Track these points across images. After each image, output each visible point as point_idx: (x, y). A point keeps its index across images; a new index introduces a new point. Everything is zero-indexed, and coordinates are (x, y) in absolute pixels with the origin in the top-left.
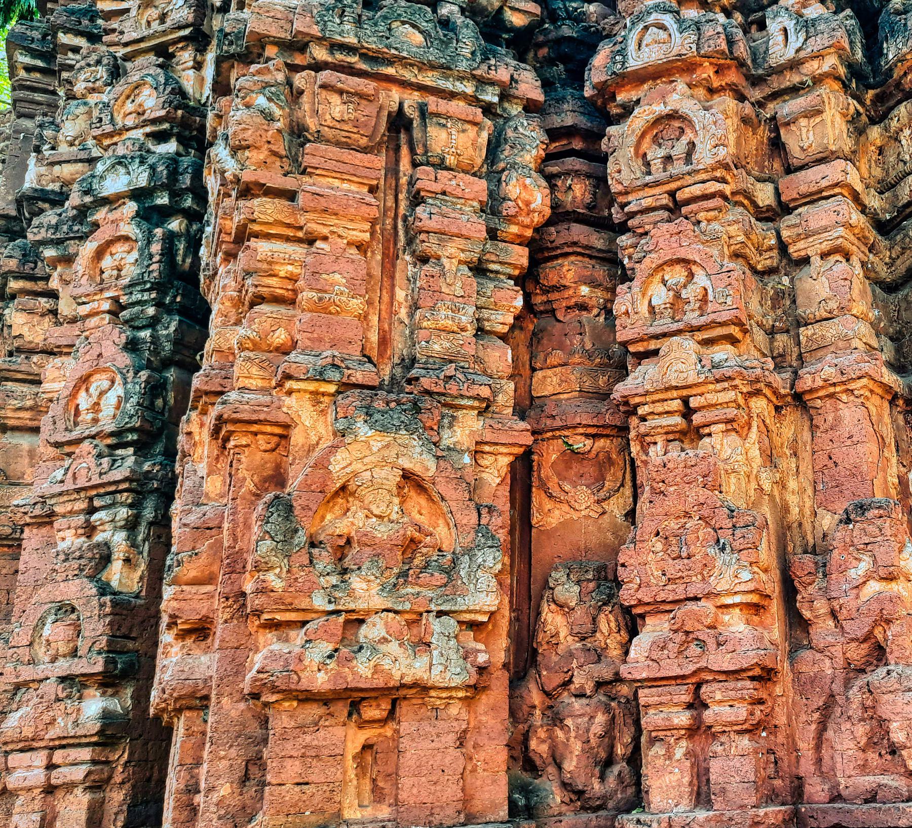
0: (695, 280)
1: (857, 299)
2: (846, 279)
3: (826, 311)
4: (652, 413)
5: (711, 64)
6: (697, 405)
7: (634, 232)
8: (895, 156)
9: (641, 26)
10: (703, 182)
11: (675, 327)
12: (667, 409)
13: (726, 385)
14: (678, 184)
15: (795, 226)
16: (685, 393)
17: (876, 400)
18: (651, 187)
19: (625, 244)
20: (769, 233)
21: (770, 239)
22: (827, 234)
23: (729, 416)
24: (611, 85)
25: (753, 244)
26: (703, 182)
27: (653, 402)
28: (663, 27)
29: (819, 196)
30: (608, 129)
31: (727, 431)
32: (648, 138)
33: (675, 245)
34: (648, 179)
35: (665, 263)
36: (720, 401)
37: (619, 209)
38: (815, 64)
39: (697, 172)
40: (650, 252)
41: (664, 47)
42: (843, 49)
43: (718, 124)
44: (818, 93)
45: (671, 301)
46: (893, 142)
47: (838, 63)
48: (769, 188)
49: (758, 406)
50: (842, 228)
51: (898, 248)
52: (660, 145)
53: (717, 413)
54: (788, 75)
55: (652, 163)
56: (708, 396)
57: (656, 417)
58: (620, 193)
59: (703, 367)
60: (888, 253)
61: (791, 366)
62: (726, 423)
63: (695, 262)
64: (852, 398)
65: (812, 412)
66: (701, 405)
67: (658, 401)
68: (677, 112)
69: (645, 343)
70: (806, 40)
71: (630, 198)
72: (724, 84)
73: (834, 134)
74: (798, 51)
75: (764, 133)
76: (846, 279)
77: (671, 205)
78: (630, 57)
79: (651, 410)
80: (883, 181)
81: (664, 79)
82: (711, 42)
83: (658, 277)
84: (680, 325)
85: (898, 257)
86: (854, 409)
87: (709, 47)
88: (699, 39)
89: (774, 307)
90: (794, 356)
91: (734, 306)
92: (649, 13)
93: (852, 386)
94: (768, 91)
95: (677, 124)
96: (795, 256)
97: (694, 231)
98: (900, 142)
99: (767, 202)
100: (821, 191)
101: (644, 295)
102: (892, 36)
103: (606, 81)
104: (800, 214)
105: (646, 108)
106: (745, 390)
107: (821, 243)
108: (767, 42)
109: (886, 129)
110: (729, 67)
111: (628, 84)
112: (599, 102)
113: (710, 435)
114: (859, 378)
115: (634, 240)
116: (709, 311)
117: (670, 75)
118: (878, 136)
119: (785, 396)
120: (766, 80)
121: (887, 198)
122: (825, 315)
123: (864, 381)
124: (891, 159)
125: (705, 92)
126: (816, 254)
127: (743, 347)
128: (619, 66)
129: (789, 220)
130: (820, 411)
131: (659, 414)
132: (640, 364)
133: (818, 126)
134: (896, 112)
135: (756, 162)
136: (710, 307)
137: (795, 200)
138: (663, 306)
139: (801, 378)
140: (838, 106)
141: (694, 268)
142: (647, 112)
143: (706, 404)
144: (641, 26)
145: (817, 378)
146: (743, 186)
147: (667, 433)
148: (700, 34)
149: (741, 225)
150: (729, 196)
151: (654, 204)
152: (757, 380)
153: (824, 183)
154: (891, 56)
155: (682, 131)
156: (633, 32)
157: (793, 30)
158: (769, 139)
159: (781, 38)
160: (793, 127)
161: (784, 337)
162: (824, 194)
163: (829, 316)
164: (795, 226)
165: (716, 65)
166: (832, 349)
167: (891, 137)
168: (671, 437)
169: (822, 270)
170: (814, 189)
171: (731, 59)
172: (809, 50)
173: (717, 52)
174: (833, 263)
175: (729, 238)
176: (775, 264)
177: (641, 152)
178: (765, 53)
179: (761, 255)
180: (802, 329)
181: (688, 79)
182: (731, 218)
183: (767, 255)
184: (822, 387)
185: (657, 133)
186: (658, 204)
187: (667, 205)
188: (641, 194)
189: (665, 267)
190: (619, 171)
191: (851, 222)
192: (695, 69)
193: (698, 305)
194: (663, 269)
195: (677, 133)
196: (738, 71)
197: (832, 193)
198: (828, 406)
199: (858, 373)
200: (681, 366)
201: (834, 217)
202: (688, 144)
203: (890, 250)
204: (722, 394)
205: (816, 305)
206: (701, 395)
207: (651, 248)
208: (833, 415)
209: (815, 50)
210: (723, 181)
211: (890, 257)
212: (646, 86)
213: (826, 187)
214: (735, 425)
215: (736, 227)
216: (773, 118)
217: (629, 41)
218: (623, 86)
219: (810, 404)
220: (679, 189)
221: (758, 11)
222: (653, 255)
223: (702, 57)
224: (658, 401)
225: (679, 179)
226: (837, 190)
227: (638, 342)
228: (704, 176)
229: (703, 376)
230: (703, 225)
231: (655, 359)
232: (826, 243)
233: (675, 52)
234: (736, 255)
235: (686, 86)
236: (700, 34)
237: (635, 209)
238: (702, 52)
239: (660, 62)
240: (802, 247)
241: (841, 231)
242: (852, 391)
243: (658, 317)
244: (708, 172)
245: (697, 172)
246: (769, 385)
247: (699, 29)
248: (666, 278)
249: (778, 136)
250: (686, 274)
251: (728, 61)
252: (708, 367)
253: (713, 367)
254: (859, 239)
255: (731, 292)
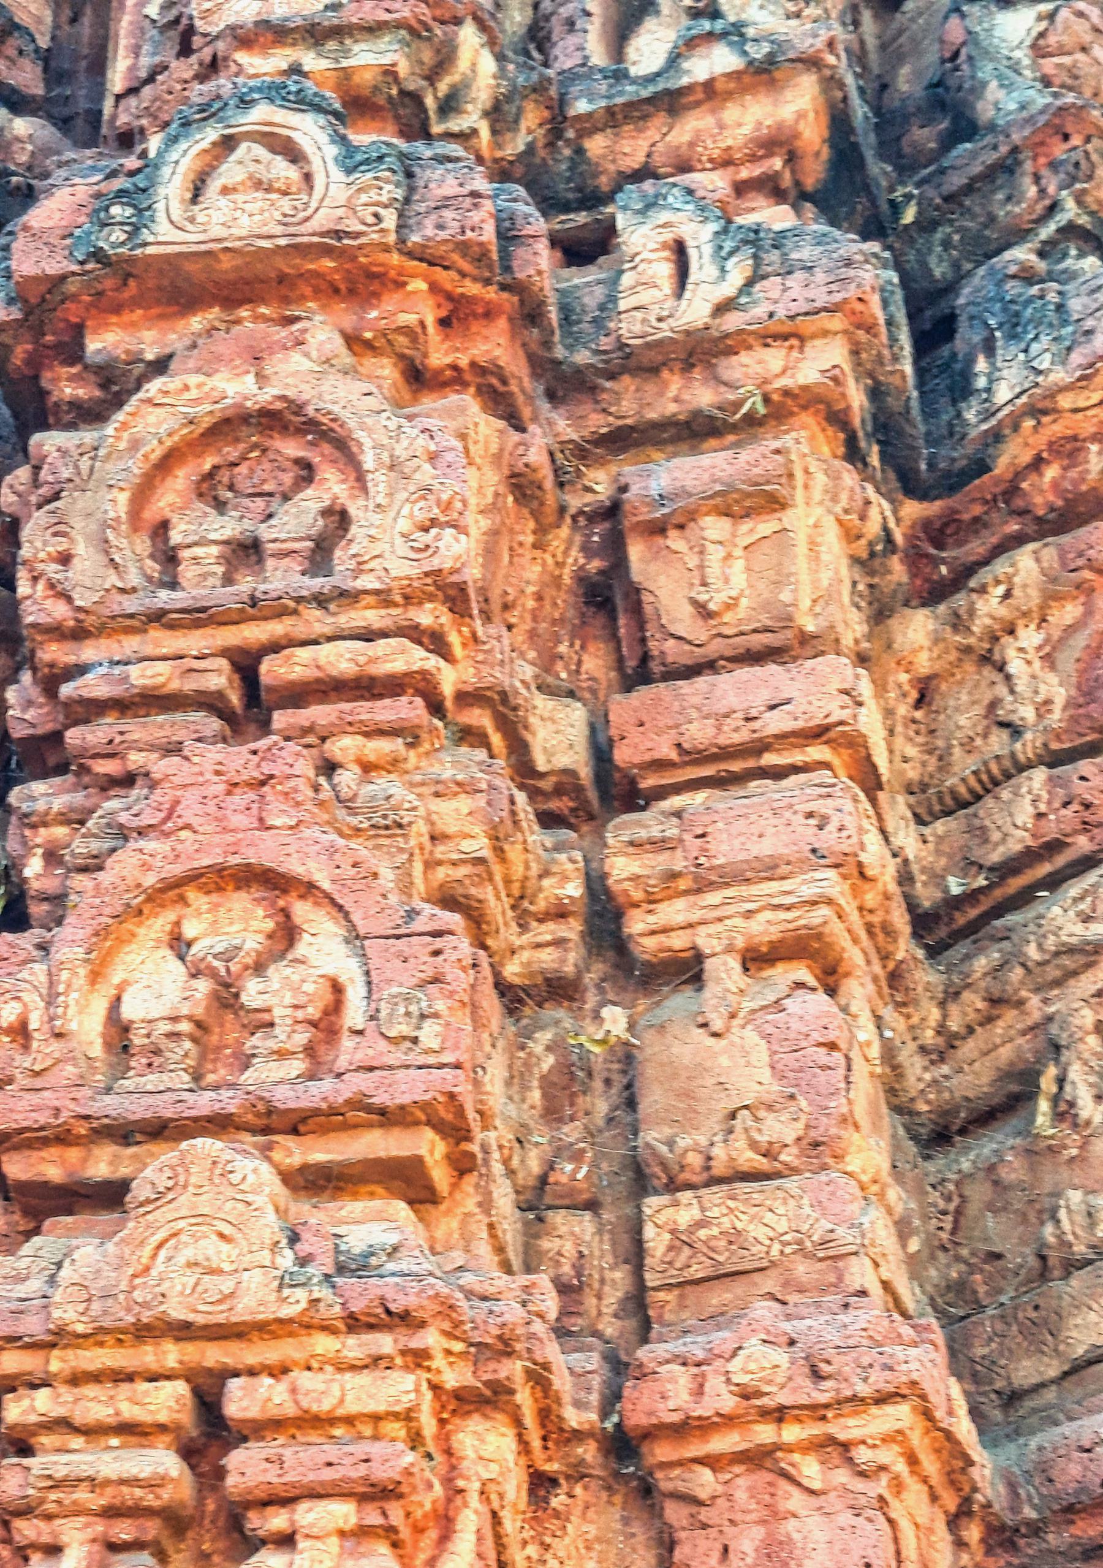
0: (301, 949)
1: (863, 1120)
2: (832, 1046)
3: (753, 1145)
4: (64, 1425)
5: (434, 288)
6: (254, 1413)
7: (84, 770)
8: (979, 710)
9: (211, 134)
10: (368, 636)
11: (204, 1103)
12: (129, 1412)
13: (385, 1343)
14: (276, 629)
15: (660, 845)
16: (214, 1355)
17: (916, 1493)
18: (172, 626)
19: (41, 806)
20: (563, 857)
21: (565, 878)
22: (774, 886)
23: (382, 1473)
24: (74, 298)
25: (508, 881)
26: (368, 636)
27: (76, 1379)
28: (292, 153)
29: (751, 763)
30: (36, 438)
31: (362, 1532)
32: (182, 478)
33: (239, 820)
34: (164, 598)
35: (193, 878)
36: (352, 1407)
37: (35, 693)
38: (774, 359)
39: (348, 597)
40: (141, 832)
41: (285, 204)
42: (870, 328)
43: (441, 463)
44: (777, 444)
45: (199, 1012)
46: (970, 667)
47: (847, 367)
48: (576, 715)
49: (488, 1451)
50: (831, 874)
51: (974, 1001)
52: (220, 506)
53: (332, 1452)
54: (675, 383)
55: (185, 554)
56: (305, 1380)
57: (77, 1442)
58: (56, 632)
59: (303, 1261)
60: (935, 1014)
61: (597, 1334)
62: (363, 1499)
63: (308, 889)
64: (842, 1476)
65: (675, 1513)
66: (274, 1412)
67: (96, 1377)
68: (298, 408)
69: (73, 1154)
70: (750, 283)
71: (88, 652)
72: (464, 362)
73: (815, 586)
74: (723, 308)
75: (566, 553)
76: (832, 1046)
77: (235, 699)
78: (161, 216)
79: (59, 1412)
80: (924, 787)
81: (263, 310)
82: (448, 214)
83: (159, 924)
84: (229, 1102)
85: (971, 1030)
86: (846, 1518)
87: (441, 227)
88: (407, 201)
89: (552, 1114)
90: (613, 1297)
91: (448, 1058)
92: (245, 103)
93: (847, 1428)
94: (598, 423)
95: (291, 448)
96: (647, 947)
97: (316, 788)
98: (1001, 667)
99: (564, 760)
100: (760, 747)
101: (96, 976)
102: (1013, 336)
103: (63, 278)
104: (678, 814)
105: (193, 380)
106: (451, 1379)
107: (749, 914)
108: (615, 281)
109: (958, 623)
110: (489, 314)
111: (135, 303)
112: (20, 354)
113: (286, 1541)
114: (882, 1399)
115: (78, 798)
116: (342, 1063)
117: (286, 301)
118: (926, 643)
119: (578, 1435)
120: (593, 390)
121: (940, 839)
122: (749, 1159)
123: (901, 1415)
124: (963, 721)
125: (397, 375)
126: (729, 949)
127: (447, 1226)
128: (118, 235)
129: (639, 824)
130: (704, 1514)
131: (93, 1432)
132: (36, 1231)
133: (765, 546)
134: (1000, 567)
135: (532, 634)
136: (348, 1052)
137: (660, 765)
138: (165, 1027)
139: (643, 1374)
140: (835, 499)
141: (302, 910)
142: (194, 394)
143: (290, 1410)
144: (211, 134)
145: (715, 1383)
146: (500, 676)
147: (111, 1513)
148: (411, 189)
149: (481, 800)
150: (449, 704)
151: (175, 685)
152: (505, 1347)
153: (776, 723)
154: (1003, 394)
155: (306, 472)
156: (183, 145)
157: (708, 250)
158: (581, 578)
159: (664, 270)
160: (675, 541)
161: (584, 1225)
162: (770, 759)
163: (763, 1164)
164: (660, 845)
165: (449, 297)
166: (769, 1283)
167: (967, 650)
168: (124, 1531)
169: (747, 1005)
170: (737, 738)
171: (504, 287)
172: (760, 311)
173: (463, 247)
174: (782, 989)
175: (433, 838)
176: (569, 969)
177: (151, 514)
178: (602, 308)
179: (523, 927)
180: (652, 1203)
181: (349, 321)
182: (447, 774)
183: (547, 931)
184: (728, 1421)
185: (216, 468)
186: (190, 685)
187: (220, 694)
188: (131, 644)
189: (191, 894)
190: (65, 559)
191: (863, 857)
192: (376, 295)
193: (302, 1037)
194: (182, 900)
195: (288, 478)
196: (513, 335)
197: (797, 757)
198: (741, 1495)
199: (879, 1380)
200: (211, 1249)
201: (807, 831)
202: (326, 513)
203: (942, 1004)
204: (363, 1379)
205: (714, 1123)
206: (279, 1371)
207: (147, 820)
208: (759, 1532)
209: (781, 313)
210: (436, 643)
211: (941, 1030)
212: (196, 322)
213: (782, 737)
214: (396, 1514)
215: (464, 803)
216: (612, 511)
217: (166, 171)
218: (117, 309)
219: (665, 1481)
220: (275, 647)
221: (577, 210)
222: (150, 845)
223: (410, 255)
224: (96, 1377)
225: (282, 613)
226: (817, 752)
227: (45, 1142)
228: (371, 617)
229: (301, 1294)
230: (347, 778)
231: (106, 1218)
232: (768, 915)
233: (321, 221)
234: (448, 901)
235: (339, 341)
236: (411, 189)
237: (102, 691)
238: (415, 238)
239: (266, 244)
240: (680, 919)
241: (830, 882)
242: (846, 1446)
243: (138, 1062)
244: (389, 603)
245: (348, 597)
246: (539, 1377)
247: (410, 175)
248: (190, 930)
249: (619, 563)
250: (270, 925)
251: (491, 293)
252: (324, 1264)
253: (341, 1269)
254: (869, 928)
255: (440, 1006)
